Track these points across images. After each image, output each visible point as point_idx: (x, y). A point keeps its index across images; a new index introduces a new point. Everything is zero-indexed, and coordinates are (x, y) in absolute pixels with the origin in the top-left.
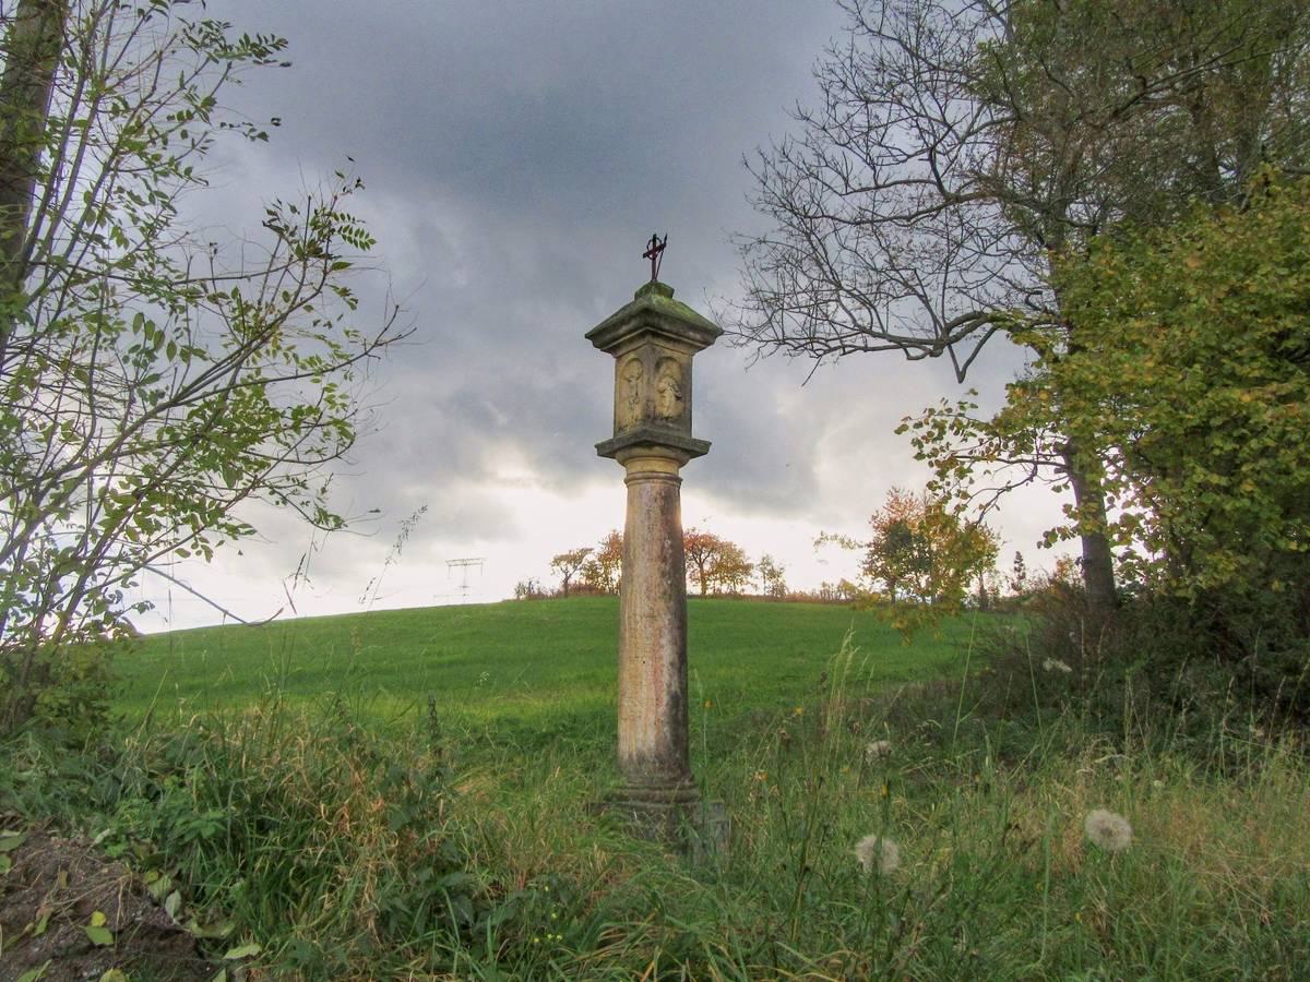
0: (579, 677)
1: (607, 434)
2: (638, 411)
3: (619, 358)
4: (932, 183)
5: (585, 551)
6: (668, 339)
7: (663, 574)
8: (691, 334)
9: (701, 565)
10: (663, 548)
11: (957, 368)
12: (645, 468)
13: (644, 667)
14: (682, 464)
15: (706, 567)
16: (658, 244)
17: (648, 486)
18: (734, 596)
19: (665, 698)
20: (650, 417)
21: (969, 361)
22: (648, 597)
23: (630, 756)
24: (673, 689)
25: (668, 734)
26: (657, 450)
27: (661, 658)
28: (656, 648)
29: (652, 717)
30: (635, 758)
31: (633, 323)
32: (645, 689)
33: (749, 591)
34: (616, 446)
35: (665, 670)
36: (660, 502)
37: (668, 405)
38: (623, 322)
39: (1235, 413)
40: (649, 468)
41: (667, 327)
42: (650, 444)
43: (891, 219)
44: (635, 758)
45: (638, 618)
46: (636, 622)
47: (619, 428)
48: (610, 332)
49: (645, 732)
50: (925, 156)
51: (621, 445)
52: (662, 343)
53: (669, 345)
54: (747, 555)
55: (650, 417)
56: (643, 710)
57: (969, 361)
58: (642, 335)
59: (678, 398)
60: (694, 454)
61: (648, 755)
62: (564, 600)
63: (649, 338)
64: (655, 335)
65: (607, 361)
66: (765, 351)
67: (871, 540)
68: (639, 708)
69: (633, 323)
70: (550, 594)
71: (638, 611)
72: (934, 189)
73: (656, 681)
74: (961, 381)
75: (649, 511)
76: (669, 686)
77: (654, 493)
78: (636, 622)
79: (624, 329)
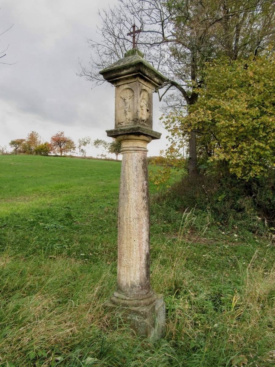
0: (33, 190)
1: (112, 127)
2: (130, 116)
3: (118, 87)
4: (161, 34)
5: (22, 140)
6: (146, 80)
7: (144, 198)
8: (156, 79)
9: (60, 147)
10: (143, 185)
11: (159, 97)
12: (134, 145)
13: (134, 243)
14: (148, 142)
15: (62, 147)
16: (136, 29)
17: (136, 154)
18: (72, 157)
19: (144, 257)
20: (136, 120)
21: (163, 95)
22: (136, 209)
23: (127, 284)
24: (147, 252)
25: (145, 273)
26: (142, 137)
27: (142, 238)
28: (140, 233)
29: (138, 266)
30: (129, 285)
31: (130, 70)
32: (135, 253)
33: (74, 155)
34: (120, 133)
35: (144, 243)
36: (142, 163)
37: (144, 115)
38: (125, 68)
39: (267, 124)
40: (137, 146)
41: (147, 74)
42: (139, 134)
43: (145, 44)
44: (129, 285)
45: (132, 219)
46: (130, 221)
47: (118, 124)
48: (115, 72)
49: (135, 274)
50: (160, 23)
51: (123, 132)
52: (142, 81)
53: (145, 84)
54: (74, 144)
55: (136, 120)
56: (134, 263)
57: (163, 95)
58: (135, 77)
59: (148, 110)
60: (154, 138)
61: (136, 283)
62: (15, 156)
63: (138, 78)
64: (142, 78)
65: (109, 88)
66: (99, 83)
67: (112, 142)
68: (132, 262)
69: (130, 70)
70: (10, 153)
71: (131, 216)
72: (161, 36)
73: (140, 249)
74: (160, 101)
75: (136, 167)
76: (145, 251)
77: (139, 158)
78: (130, 221)
79: (125, 71)
